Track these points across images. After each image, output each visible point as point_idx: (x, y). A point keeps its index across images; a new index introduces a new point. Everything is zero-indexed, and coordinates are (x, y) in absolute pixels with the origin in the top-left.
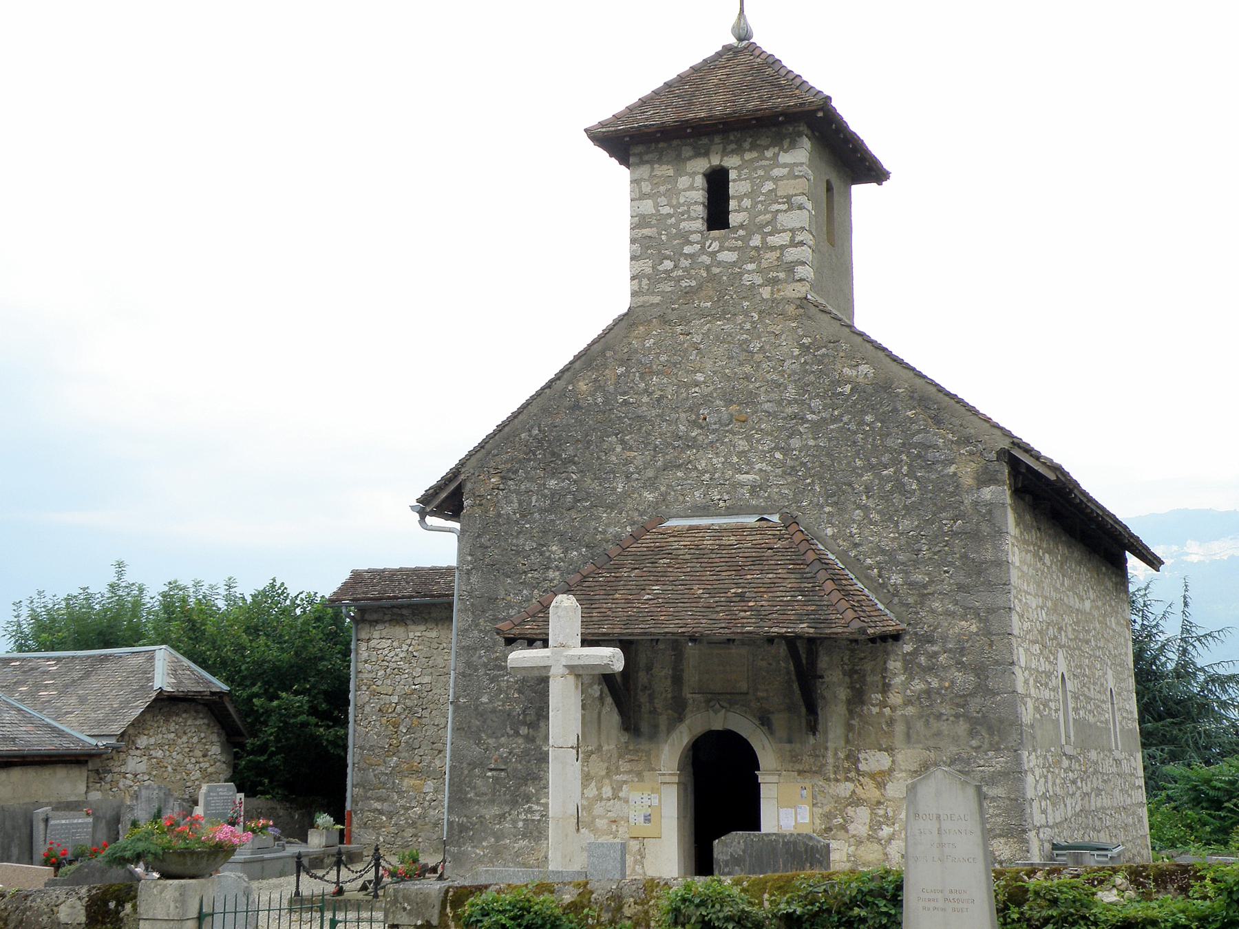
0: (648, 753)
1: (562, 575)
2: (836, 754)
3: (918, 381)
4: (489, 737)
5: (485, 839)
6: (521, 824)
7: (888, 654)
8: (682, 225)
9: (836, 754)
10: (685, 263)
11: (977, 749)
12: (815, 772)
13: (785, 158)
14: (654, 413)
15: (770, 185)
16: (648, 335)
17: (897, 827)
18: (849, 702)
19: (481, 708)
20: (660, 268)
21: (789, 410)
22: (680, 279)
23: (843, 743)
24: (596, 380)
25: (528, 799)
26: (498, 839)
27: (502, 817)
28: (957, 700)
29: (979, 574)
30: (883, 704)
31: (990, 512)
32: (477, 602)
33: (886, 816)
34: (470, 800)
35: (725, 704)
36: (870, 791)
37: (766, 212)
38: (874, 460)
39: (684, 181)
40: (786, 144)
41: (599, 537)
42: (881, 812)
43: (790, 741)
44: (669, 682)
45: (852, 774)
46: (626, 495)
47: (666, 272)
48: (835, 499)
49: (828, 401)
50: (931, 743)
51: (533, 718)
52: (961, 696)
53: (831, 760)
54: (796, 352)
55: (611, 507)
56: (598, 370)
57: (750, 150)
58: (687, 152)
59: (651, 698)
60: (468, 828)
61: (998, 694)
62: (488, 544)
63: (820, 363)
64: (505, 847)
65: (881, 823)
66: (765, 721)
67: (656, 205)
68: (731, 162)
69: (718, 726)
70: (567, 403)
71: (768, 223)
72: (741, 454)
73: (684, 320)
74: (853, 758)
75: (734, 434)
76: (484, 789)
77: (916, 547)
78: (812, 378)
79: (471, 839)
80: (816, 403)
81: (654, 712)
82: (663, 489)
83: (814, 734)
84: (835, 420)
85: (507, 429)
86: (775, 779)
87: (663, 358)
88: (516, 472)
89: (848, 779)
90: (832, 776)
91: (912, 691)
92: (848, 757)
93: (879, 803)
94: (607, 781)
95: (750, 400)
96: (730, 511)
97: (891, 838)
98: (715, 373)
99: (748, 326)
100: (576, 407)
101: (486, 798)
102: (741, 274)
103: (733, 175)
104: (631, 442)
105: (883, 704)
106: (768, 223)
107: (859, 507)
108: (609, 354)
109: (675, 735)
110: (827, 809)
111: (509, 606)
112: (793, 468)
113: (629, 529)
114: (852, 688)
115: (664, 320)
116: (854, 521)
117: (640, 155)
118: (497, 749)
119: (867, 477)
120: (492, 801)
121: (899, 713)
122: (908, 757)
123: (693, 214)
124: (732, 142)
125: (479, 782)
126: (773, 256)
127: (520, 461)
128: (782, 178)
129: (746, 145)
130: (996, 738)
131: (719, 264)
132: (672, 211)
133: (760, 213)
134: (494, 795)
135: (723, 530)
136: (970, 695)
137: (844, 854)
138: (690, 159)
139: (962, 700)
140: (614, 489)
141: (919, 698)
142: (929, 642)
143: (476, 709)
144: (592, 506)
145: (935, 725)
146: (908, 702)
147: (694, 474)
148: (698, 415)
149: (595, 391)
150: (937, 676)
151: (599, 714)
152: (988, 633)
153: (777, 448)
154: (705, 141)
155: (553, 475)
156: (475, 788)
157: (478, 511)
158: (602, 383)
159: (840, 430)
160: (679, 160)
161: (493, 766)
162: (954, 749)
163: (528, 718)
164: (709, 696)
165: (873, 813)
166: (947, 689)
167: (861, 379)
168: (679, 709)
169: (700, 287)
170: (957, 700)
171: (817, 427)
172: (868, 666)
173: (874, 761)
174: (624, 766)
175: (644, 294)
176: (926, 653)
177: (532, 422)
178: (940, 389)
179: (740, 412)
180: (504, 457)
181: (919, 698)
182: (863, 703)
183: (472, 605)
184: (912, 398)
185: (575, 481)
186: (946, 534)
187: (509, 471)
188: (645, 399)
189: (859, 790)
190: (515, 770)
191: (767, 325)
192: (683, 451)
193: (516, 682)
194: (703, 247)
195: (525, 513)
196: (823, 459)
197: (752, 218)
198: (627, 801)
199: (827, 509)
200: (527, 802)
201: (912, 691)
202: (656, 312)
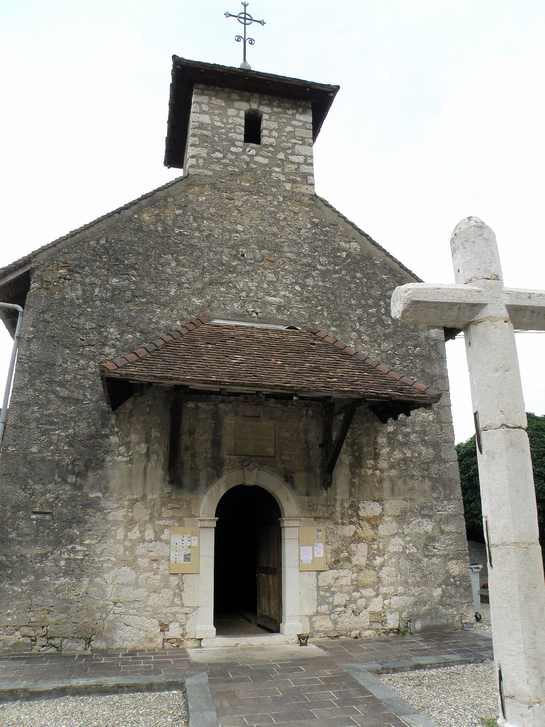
0: (189, 503)
1: (117, 351)
2: (342, 504)
3: (388, 259)
4: (35, 483)
5: (24, 577)
6: (63, 563)
7: (377, 432)
8: (230, 135)
9: (342, 504)
10: (230, 156)
11: (437, 499)
12: (327, 518)
13: (298, 117)
14: (203, 244)
15: (289, 129)
16: (201, 193)
17: (386, 557)
18: (351, 466)
19: (29, 457)
20: (213, 155)
21: (305, 260)
22: (226, 165)
23: (347, 495)
24: (157, 215)
25: (72, 540)
26: (38, 576)
27: (44, 556)
28: (423, 466)
29: (432, 383)
30: (375, 468)
31: (435, 345)
32: (34, 365)
33: (378, 549)
34: (12, 540)
35: (256, 464)
36: (367, 532)
37: (287, 142)
38: (363, 302)
39: (231, 112)
40: (300, 110)
41: (152, 326)
42: (375, 547)
43: (308, 494)
44: (209, 445)
45: (354, 519)
46: (177, 298)
47: (217, 158)
48: (338, 322)
49: (331, 259)
50: (408, 496)
51: (82, 468)
52: (426, 463)
53: (338, 509)
54: (309, 226)
55: (165, 305)
56: (160, 209)
57: (277, 107)
58: (235, 96)
59: (193, 457)
60: (7, 566)
61: (448, 462)
62: (51, 320)
63: (325, 235)
64: (46, 584)
65: (374, 555)
66: (288, 479)
67: (212, 119)
68: (265, 110)
69: (250, 482)
70: (132, 226)
71: (289, 148)
72: (270, 283)
73: (228, 189)
74: (354, 507)
75: (265, 269)
76: (26, 531)
77: (393, 361)
78: (320, 243)
79: (10, 577)
80: (323, 259)
81: (194, 468)
82: (208, 298)
83: (326, 489)
84: (336, 272)
85: (78, 236)
86: (297, 523)
87: (212, 210)
88: (83, 268)
89: (351, 523)
90: (340, 521)
91: (394, 459)
92: (351, 507)
93: (374, 540)
94: (150, 526)
95: (277, 249)
96: (261, 320)
97: (382, 566)
98: (251, 227)
99: (276, 203)
100: (139, 229)
101: (28, 539)
102: (271, 172)
103: (265, 117)
104: (184, 261)
105: (375, 468)
106: (289, 148)
107: (354, 330)
108: (169, 199)
109: (214, 488)
110: (335, 546)
111: (65, 371)
112: (308, 298)
113: (178, 323)
114: (353, 455)
115: (213, 186)
116: (351, 339)
117: (202, 90)
118: (43, 494)
119: (359, 311)
120: (35, 542)
121: (386, 474)
122: (393, 506)
123: (237, 130)
124: (265, 99)
125: (22, 524)
126: (293, 167)
127: (87, 261)
128: (298, 127)
129: (275, 104)
130: (448, 492)
131: (255, 163)
132: (223, 125)
133: (284, 142)
134: (37, 536)
135: (247, 328)
136: (431, 462)
137: (349, 579)
138: (237, 101)
139: (426, 466)
140: (168, 292)
141: (399, 464)
142: (404, 425)
143: (25, 457)
144: (147, 302)
145: (410, 483)
146: (392, 466)
147: (234, 291)
148: (238, 251)
149: (157, 222)
150: (410, 449)
151: (145, 468)
152: (440, 422)
153: (296, 283)
154: (247, 94)
155: (115, 275)
156: (17, 529)
157: (44, 293)
158: (163, 218)
159: (340, 279)
160: (229, 100)
161: (38, 510)
162: (422, 500)
163: (77, 468)
164: (244, 458)
165: (370, 548)
166: (416, 458)
167: (352, 250)
168: (217, 468)
169: (241, 173)
170: (423, 466)
171: (324, 275)
172: (364, 441)
173: (369, 509)
174: (166, 513)
175: (199, 168)
176: (402, 433)
177: (100, 235)
178: (402, 266)
179: (270, 255)
180: (73, 256)
181: (399, 464)
182: (361, 467)
183: (30, 367)
184: (385, 268)
185: (134, 282)
186: (410, 355)
187: (76, 266)
188: (197, 234)
189: (359, 531)
190: (60, 514)
191: (289, 206)
192: (225, 274)
193: (67, 436)
194: (244, 150)
195: (88, 299)
196: (330, 295)
197: (279, 143)
198: (168, 543)
199: (333, 329)
200: (71, 543)
201: (394, 459)
202: (208, 181)
